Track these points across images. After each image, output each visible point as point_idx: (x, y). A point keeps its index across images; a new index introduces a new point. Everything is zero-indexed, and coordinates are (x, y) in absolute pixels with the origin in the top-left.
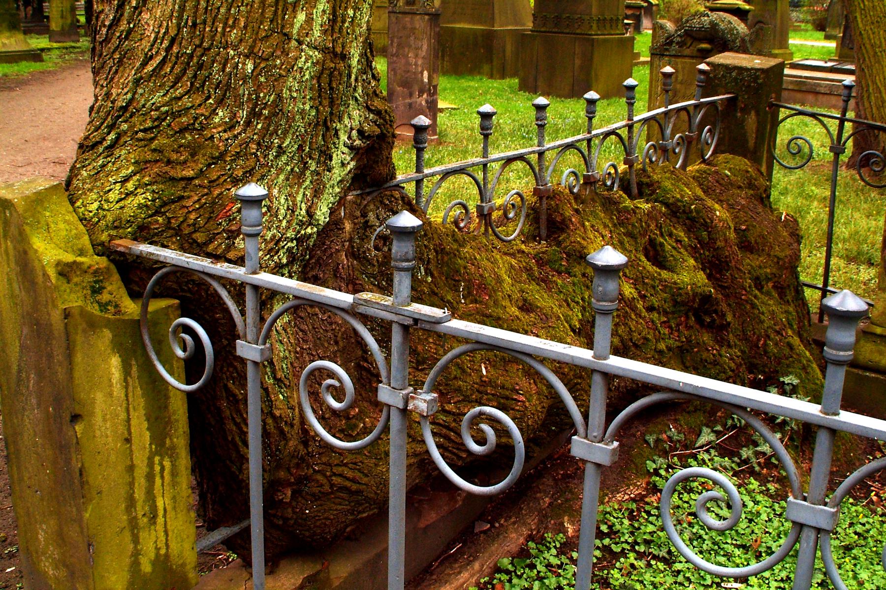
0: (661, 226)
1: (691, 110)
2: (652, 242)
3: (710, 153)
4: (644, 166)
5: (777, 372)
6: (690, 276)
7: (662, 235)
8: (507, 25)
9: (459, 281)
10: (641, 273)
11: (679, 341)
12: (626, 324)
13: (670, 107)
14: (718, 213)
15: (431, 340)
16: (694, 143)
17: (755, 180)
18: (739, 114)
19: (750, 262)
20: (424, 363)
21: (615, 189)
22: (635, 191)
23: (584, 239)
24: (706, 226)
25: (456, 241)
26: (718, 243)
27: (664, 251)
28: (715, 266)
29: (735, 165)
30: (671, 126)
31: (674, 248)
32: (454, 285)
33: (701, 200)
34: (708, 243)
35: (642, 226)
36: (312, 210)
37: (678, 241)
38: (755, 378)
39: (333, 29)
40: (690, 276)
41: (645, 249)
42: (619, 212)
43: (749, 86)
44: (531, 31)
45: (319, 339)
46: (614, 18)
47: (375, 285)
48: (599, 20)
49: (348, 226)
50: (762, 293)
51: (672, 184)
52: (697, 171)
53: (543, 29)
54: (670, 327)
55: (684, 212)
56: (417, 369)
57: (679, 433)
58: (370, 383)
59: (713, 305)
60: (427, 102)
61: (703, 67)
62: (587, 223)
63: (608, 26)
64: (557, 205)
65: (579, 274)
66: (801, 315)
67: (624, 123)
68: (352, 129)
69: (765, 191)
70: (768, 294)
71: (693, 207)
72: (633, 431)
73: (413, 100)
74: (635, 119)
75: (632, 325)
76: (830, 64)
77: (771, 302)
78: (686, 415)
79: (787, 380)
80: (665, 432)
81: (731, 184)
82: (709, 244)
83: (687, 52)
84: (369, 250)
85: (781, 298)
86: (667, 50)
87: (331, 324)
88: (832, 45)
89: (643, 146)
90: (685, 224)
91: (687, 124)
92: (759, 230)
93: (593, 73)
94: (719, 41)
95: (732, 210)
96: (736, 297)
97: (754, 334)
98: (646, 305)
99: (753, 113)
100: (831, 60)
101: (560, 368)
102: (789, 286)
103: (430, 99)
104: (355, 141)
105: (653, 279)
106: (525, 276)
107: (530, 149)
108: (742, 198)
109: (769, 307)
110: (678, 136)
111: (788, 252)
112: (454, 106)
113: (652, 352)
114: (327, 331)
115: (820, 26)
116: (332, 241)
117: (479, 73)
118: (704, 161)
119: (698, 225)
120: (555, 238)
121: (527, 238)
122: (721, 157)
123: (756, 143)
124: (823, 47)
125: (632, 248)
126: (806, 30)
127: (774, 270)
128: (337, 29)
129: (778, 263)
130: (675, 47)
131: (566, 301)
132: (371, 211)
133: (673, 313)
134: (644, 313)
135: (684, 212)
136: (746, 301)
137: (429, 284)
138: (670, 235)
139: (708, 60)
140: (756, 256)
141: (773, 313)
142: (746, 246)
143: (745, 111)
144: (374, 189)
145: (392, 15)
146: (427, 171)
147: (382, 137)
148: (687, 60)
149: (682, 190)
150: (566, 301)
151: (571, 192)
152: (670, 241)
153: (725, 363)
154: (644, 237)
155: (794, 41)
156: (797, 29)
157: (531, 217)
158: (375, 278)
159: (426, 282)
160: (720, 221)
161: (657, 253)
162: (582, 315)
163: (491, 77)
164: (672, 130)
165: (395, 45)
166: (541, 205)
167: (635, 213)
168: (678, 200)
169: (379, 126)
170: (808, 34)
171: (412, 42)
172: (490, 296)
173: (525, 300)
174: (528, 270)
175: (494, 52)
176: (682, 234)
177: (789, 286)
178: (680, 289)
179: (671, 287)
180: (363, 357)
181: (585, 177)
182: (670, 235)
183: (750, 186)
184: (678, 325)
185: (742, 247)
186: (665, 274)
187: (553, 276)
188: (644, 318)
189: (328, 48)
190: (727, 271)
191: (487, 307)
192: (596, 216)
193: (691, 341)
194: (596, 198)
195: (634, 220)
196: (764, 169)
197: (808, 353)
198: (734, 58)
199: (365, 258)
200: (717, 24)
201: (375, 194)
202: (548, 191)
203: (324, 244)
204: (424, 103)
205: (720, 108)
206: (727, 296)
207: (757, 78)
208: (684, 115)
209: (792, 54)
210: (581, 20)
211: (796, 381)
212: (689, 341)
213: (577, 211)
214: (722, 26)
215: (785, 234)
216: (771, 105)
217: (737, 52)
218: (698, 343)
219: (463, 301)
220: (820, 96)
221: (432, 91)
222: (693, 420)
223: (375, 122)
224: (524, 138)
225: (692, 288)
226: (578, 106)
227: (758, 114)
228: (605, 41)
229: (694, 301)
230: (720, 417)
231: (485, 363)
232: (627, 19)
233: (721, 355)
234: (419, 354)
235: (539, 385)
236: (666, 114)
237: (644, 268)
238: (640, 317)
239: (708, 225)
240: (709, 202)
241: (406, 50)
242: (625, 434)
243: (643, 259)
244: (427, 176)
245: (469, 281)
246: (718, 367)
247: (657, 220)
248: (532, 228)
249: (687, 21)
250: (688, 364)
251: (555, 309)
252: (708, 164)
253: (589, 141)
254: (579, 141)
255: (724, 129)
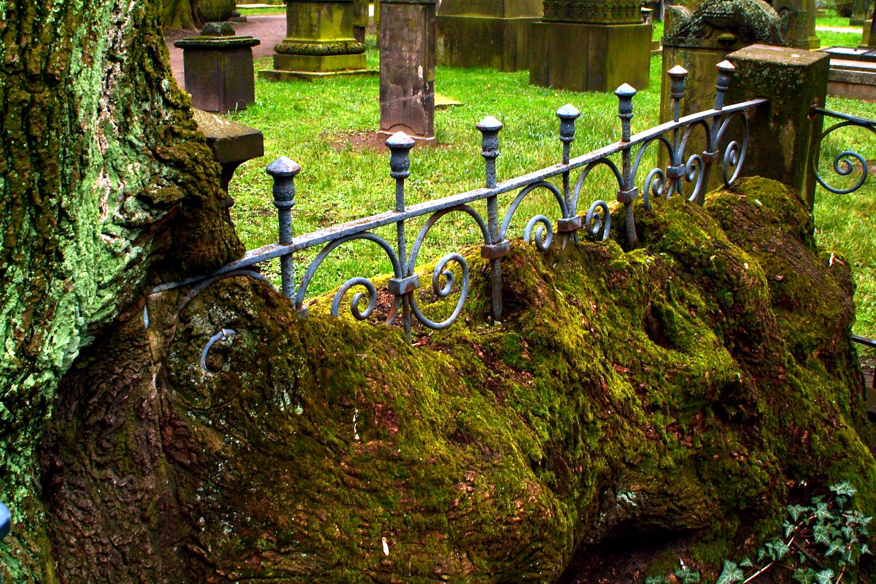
0: (668, 288)
1: (710, 122)
2: (656, 311)
3: (735, 176)
4: (646, 201)
5: (826, 477)
6: (709, 357)
7: (669, 300)
8: (519, 15)
9: (351, 407)
10: (640, 358)
11: (693, 447)
12: (615, 439)
13: (682, 120)
14: (746, 266)
15: (300, 507)
16: (714, 167)
17: (794, 211)
18: (772, 125)
19: (792, 324)
20: (287, 543)
21: (605, 237)
22: (633, 236)
23: (554, 319)
24: (730, 284)
25: (349, 342)
26: (747, 307)
27: (672, 322)
28: (742, 338)
29: (768, 192)
30: (683, 145)
31: (686, 317)
32: (344, 414)
33: (724, 247)
34: (733, 307)
35: (641, 291)
36: (32, 348)
37: (692, 307)
38: (796, 485)
39: (19, 28)
40: (709, 357)
41: (646, 320)
42: (609, 272)
43: (785, 87)
44: (543, 21)
45: (115, 517)
46: (630, 5)
47: (208, 425)
48: (614, 8)
49: (154, 340)
50: (804, 365)
51: (685, 226)
52: (719, 200)
53: (554, 19)
54: (681, 431)
55: (700, 265)
56: (278, 552)
57: (693, 570)
58: (204, 575)
59: (740, 394)
60: (422, 99)
61: (726, 65)
62: (560, 293)
63: (624, 14)
64: (516, 270)
65: (546, 372)
66: (854, 387)
67: (617, 145)
68: (126, 195)
69: (807, 225)
70: (812, 366)
71: (712, 258)
72: (629, 569)
73: (408, 98)
74: (633, 139)
75: (625, 438)
76: (860, 52)
77: (817, 379)
78: (704, 547)
79: (839, 489)
80: (674, 571)
81: (763, 218)
82: (735, 309)
83: (706, 43)
84: (195, 373)
85: (829, 371)
86: (682, 41)
87: (134, 492)
88: (859, 31)
89: (646, 171)
90: (702, 282)
91: (705, 140)
92: (800, 280)
93: (608, 65)
94: (743, 29)
95: (764, 254)
96: (771, 376)
97: (795, 425)
98: (647, 403)
99: (790, 122)
100: (860, 48)
101: (508, 531)
102: (839, 354)
103: (425, 97)
104: (133, 215)
105: (657, 365)
106: (463, 382)
107: (473, 193)
108: (777, 236)
109: (815, 386)
110: (692, 157)
111: (838, 311)
112: (457, 102)
113: (654, 472)
114: (127, 504)
115: (845, 12)
116: (126, 368)
117: (489, 66)
118: (727, 187)
119: (719, 283)
120: (513, 317)
121: (474, 317)
122: (750, 181)
123: (793, 161)
124: (849, 33)
125: (628, 323)
126: (831, 17)
127: (820, 335)
128: (28, 28)
129: (826, 324)
130: (691, 37)
131: (525, 416)
132: (195, 313)
133: (684, 410)
134: (643, 418)
135: (700, 265)
136: (784, 381)
137: (299, 418)
138: (682, 298)
139: (731, 55)
140: (797, 316)
141: (819, 395)
142: (783, 302)
143: (780, 120)
144: (200, 278)
145: (384, 5)
146: (296, 241)
147: (193, 202)
148: (707, 53)
149: (698, 234)
150: (525, 416)
151: (540, 248)
152: (681, 308)
153: (756, 473)
154: (644, 303)
155: (820, 27)
156: (822, 16)
157: (481, 285)
158: (208, 416)
159: (294, 415)
160: (749, 276)
161: (662, 326)
162: (550, 434)
163: (502, 69)
164: (685, 150)
165: (388, 37)
166: (493, 270)
167: (631, 272)
168: (692, 249)
169: (183, 185)
170: (833, 20)
171: (405, 35)
172: (400, 427)
173: (460, 424)
174: (469, 372)
175: (505, 43)
176: (697, 297)
177: (839, 354)
178: (694, 377)
179: (681, 375)
180: (192, 536)
181: (560, 224)
182: (682, 298)
183: (788, 218)
184: (691, 426)
185: (778, 304)
186: (673, 357)
187: (508, 377)
188: (643, 426)
189: (12, 65)
190: (759, 343)
191: (396, 445)
192: (575, 280)
193: (709, 446)
194: (576, 253)
195: (630, 282)
196: (803, 194)
197: (866, 450)
198: (765, 52)
199: (190, 386)
200: (741, 10)
201: (204, 285)
202: (502, 250)
203: (112, 372)
204: (419, 101)
205: (747, 117)
206: (758, 376)
207: (796, 77)
208: (700, 128)
209: (819, 41)
210: (596, 8)
211: (851, 491)
212: (706, 445)
213: (545, 278)
214: (748, 11)
215: (835, 285)
216: (813, 112)
217: (766, 43)
218: (719, 448)
219: (357, 437)
220: (851, 87)
221: (428, 88)
222: (713, 552)
223: (175, 180)
224: (530, 137)
225: (710, 375)
226: (591, 100)
227: (796, 124)
228: (619, 29)
229: (714, 391)
230: (749, 546)
231: (388, 536)
232: (646, 6)
233: (750, 463)
234: (280, 530)
235: (476, 560)
236: (675, 129)
237: (644, 350)
238: (637, 424)
239: (733, 283)
240: (735, 250)
241: (400, 42)
242: (618, 573)
243: (643, 336)
244: (297, 249)
245: (366, 405)
246: (746, 479)
247: (662, 279)
248: (481, 302)
249: (706, 6)
250: (705, 477)
251: (507, 434)
252: (732, 191)
253: (566, 174)
254: (549, 176)
255: (752, 143)
